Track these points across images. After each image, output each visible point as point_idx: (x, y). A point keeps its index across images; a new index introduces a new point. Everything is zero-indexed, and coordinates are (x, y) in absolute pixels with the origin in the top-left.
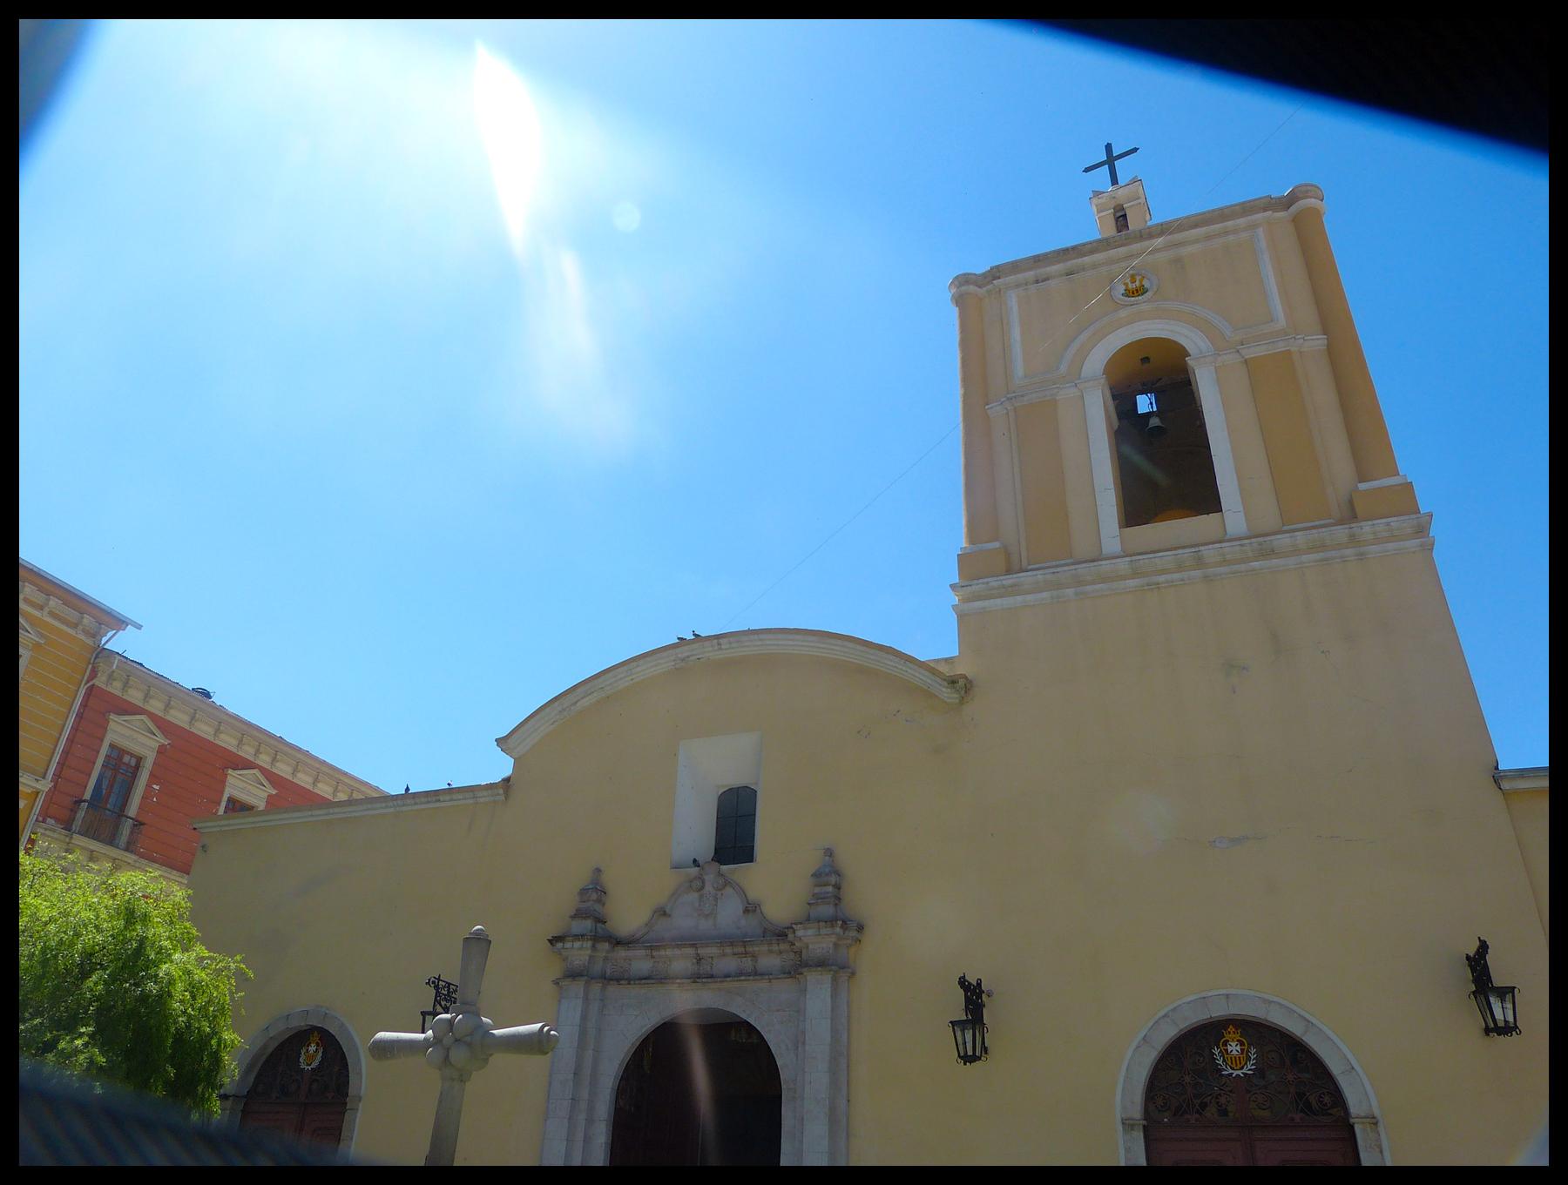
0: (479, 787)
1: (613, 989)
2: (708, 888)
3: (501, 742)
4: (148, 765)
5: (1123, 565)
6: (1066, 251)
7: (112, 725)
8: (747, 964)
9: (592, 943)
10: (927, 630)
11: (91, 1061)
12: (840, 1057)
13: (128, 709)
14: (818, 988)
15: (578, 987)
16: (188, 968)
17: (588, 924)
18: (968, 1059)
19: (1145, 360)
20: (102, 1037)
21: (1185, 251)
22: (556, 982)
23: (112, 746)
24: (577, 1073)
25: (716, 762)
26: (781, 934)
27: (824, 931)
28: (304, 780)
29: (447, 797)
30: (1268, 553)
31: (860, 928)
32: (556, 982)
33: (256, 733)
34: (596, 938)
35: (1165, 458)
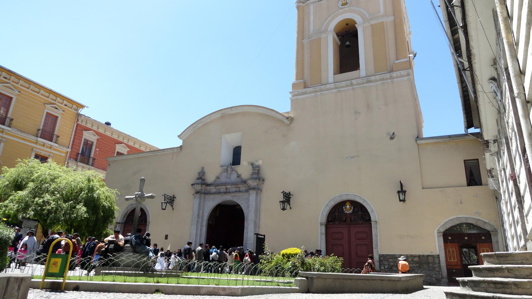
0: (174, 148)
1: (206, 196)
2: (229, 171)
3: (179, 136)
4: (95, 144)
5: (332, 86)
7: (84, 134)
8: (238, 189)
9: (202, 185)
10: (283, 105)
12: (258, 211)
13: (87, 129)
14: (253, 194)
15: (198, 195)
16: (105, 193)
17: (200, 181)
19: (347, 24)
20: (85, 205)
22: (193, 195)
23: (85, 139)
24: (198, 216)
25: (232, 139)
26: (245, 182)
28: (137, 146)
30: (369, 82)
31: (263, 180)
32: (193, 195)
33: (307, 56)
34: (202, 184)
35: (348, 54)
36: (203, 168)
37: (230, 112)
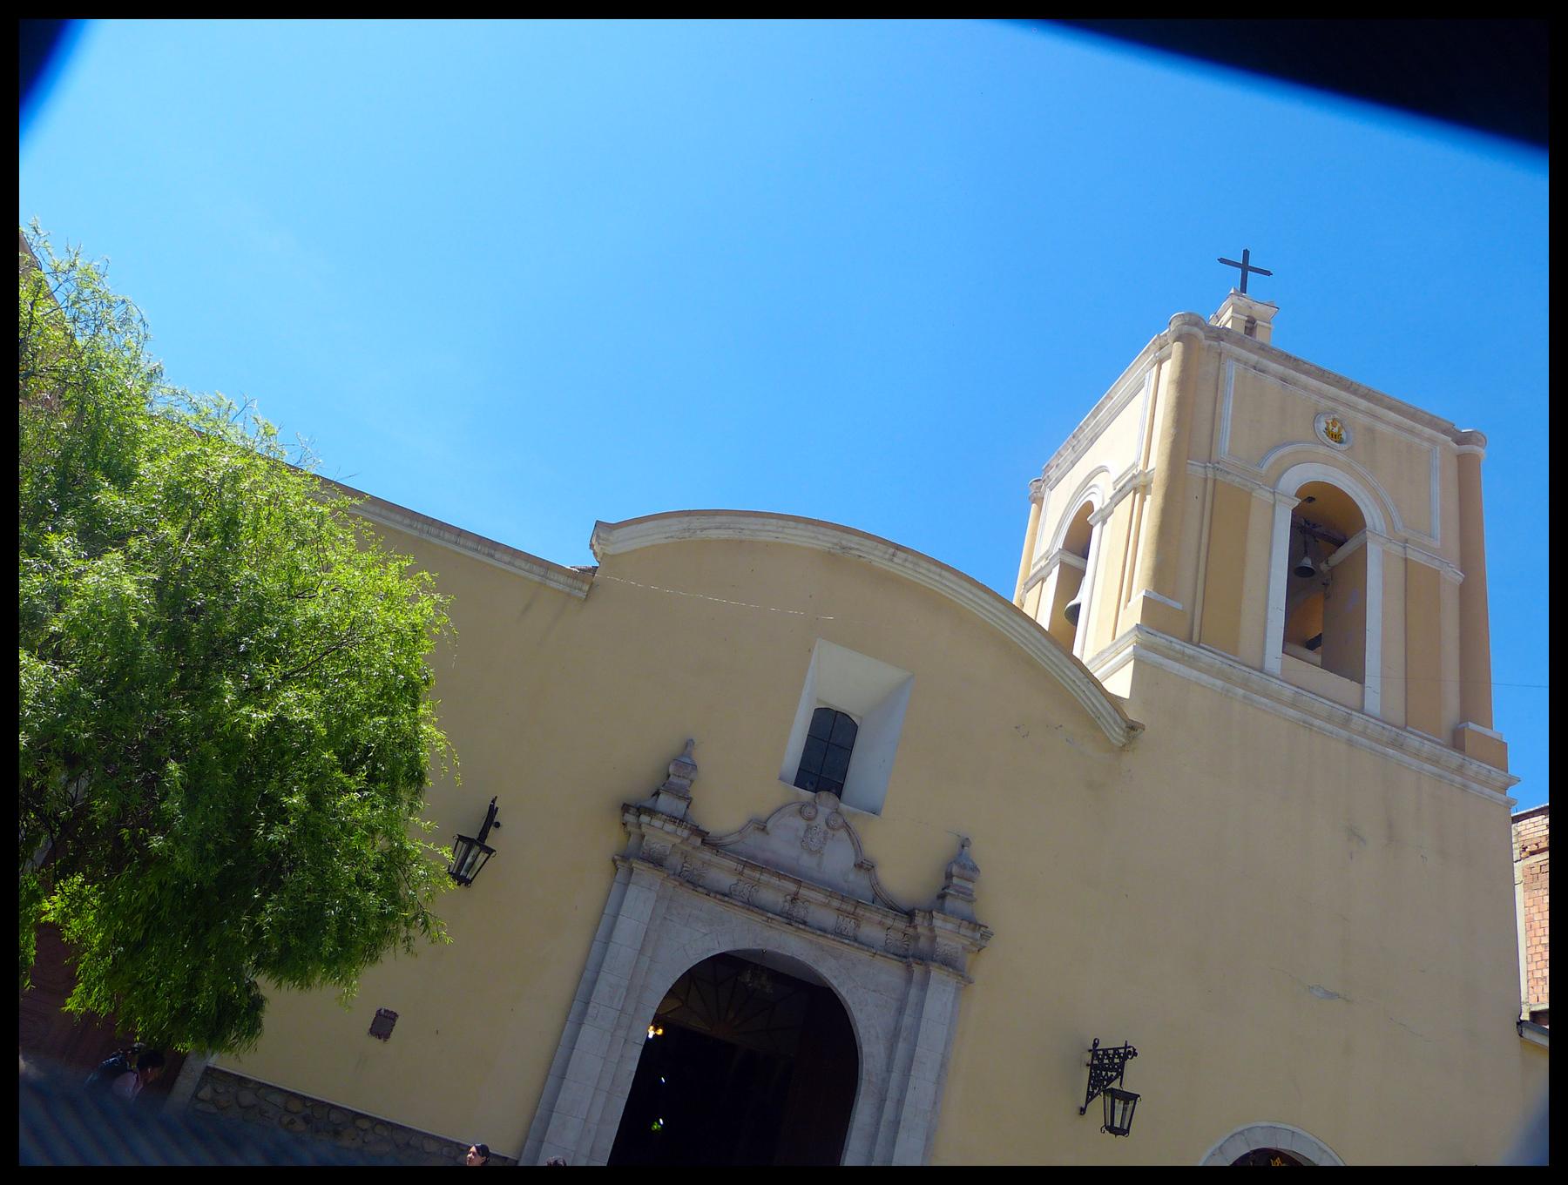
2: (820, 821)
6: (1288, 357)
8: (848, 925)
9: (656, 824)
11: (279, 814)
18: (1112, 1129)
21: (1380, 427)
25: (843, 677)
27: (963, 931)
29: (507, 558)
31: (987, 936)
36: (689, 744)
37: (879, 559)
